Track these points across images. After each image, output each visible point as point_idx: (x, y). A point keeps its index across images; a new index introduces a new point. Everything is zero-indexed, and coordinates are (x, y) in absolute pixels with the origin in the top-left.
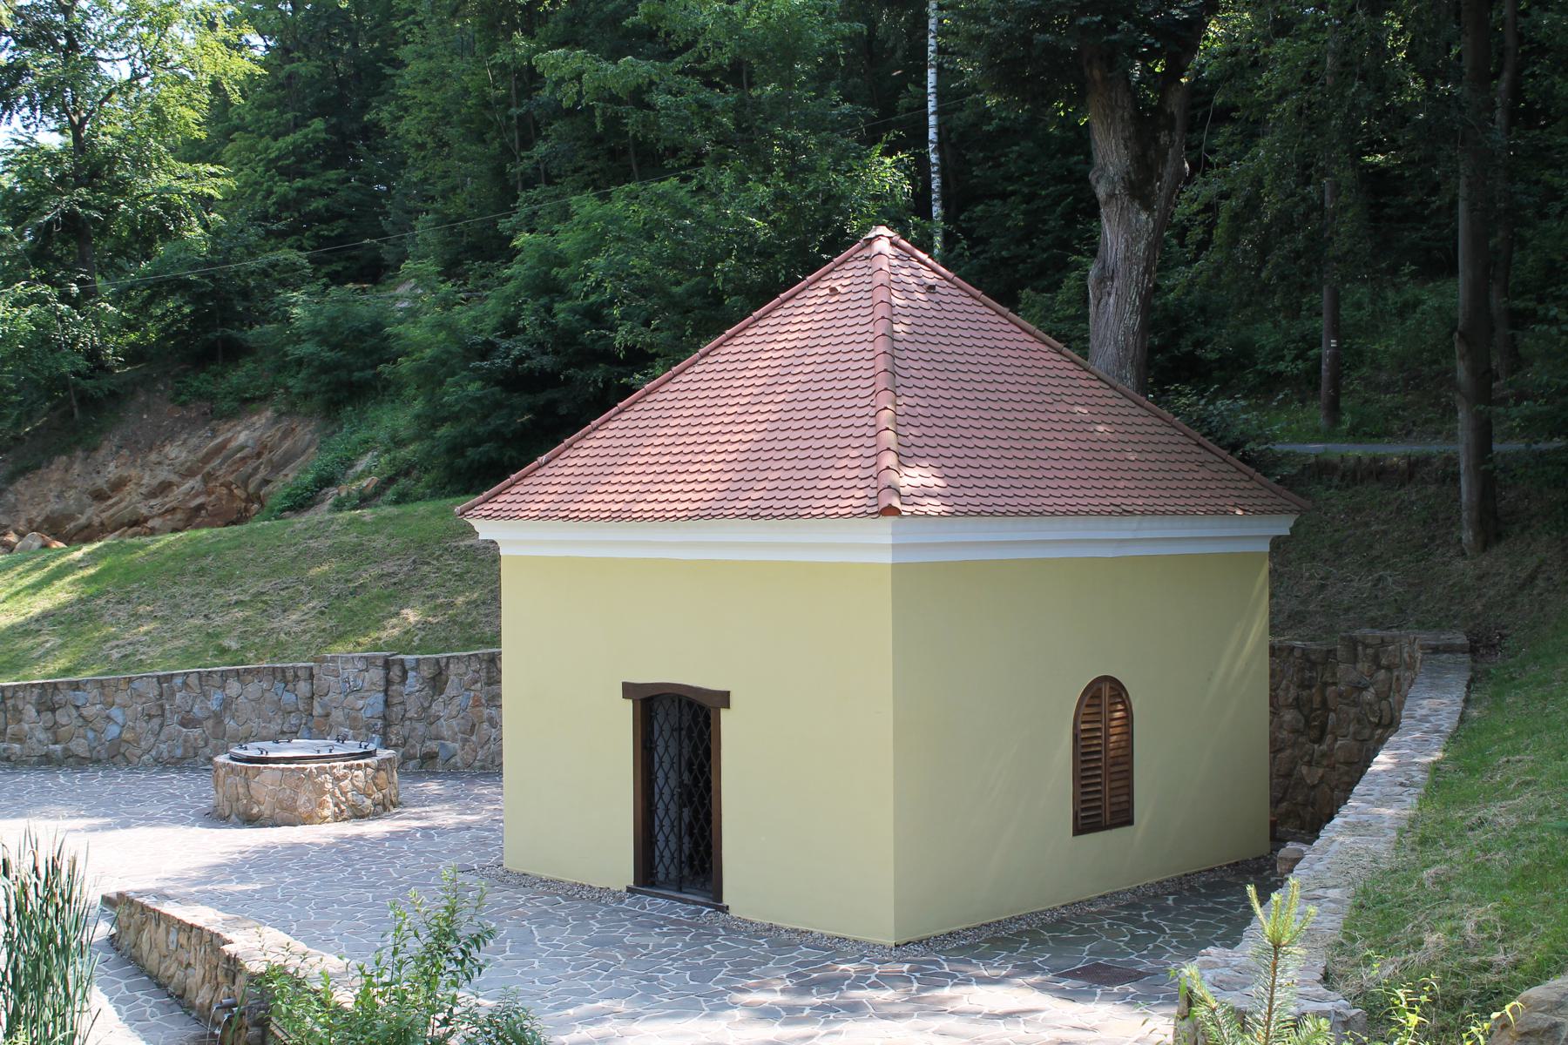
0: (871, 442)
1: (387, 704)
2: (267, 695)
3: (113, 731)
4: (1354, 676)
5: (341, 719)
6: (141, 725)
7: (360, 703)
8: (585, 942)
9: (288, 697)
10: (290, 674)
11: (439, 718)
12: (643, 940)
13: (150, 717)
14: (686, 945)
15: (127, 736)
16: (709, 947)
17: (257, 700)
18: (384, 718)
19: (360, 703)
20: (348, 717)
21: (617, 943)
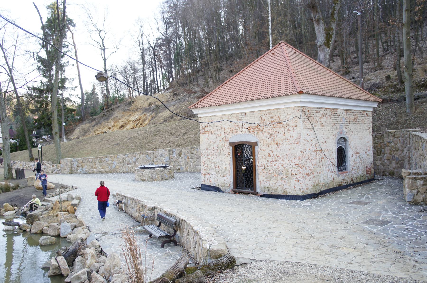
3: (114, 166)
4: (388, 140)
7: (164, 159)
9: (149, 158)
10: (149, 153)
15: (117, 167)
19: (164, 159)
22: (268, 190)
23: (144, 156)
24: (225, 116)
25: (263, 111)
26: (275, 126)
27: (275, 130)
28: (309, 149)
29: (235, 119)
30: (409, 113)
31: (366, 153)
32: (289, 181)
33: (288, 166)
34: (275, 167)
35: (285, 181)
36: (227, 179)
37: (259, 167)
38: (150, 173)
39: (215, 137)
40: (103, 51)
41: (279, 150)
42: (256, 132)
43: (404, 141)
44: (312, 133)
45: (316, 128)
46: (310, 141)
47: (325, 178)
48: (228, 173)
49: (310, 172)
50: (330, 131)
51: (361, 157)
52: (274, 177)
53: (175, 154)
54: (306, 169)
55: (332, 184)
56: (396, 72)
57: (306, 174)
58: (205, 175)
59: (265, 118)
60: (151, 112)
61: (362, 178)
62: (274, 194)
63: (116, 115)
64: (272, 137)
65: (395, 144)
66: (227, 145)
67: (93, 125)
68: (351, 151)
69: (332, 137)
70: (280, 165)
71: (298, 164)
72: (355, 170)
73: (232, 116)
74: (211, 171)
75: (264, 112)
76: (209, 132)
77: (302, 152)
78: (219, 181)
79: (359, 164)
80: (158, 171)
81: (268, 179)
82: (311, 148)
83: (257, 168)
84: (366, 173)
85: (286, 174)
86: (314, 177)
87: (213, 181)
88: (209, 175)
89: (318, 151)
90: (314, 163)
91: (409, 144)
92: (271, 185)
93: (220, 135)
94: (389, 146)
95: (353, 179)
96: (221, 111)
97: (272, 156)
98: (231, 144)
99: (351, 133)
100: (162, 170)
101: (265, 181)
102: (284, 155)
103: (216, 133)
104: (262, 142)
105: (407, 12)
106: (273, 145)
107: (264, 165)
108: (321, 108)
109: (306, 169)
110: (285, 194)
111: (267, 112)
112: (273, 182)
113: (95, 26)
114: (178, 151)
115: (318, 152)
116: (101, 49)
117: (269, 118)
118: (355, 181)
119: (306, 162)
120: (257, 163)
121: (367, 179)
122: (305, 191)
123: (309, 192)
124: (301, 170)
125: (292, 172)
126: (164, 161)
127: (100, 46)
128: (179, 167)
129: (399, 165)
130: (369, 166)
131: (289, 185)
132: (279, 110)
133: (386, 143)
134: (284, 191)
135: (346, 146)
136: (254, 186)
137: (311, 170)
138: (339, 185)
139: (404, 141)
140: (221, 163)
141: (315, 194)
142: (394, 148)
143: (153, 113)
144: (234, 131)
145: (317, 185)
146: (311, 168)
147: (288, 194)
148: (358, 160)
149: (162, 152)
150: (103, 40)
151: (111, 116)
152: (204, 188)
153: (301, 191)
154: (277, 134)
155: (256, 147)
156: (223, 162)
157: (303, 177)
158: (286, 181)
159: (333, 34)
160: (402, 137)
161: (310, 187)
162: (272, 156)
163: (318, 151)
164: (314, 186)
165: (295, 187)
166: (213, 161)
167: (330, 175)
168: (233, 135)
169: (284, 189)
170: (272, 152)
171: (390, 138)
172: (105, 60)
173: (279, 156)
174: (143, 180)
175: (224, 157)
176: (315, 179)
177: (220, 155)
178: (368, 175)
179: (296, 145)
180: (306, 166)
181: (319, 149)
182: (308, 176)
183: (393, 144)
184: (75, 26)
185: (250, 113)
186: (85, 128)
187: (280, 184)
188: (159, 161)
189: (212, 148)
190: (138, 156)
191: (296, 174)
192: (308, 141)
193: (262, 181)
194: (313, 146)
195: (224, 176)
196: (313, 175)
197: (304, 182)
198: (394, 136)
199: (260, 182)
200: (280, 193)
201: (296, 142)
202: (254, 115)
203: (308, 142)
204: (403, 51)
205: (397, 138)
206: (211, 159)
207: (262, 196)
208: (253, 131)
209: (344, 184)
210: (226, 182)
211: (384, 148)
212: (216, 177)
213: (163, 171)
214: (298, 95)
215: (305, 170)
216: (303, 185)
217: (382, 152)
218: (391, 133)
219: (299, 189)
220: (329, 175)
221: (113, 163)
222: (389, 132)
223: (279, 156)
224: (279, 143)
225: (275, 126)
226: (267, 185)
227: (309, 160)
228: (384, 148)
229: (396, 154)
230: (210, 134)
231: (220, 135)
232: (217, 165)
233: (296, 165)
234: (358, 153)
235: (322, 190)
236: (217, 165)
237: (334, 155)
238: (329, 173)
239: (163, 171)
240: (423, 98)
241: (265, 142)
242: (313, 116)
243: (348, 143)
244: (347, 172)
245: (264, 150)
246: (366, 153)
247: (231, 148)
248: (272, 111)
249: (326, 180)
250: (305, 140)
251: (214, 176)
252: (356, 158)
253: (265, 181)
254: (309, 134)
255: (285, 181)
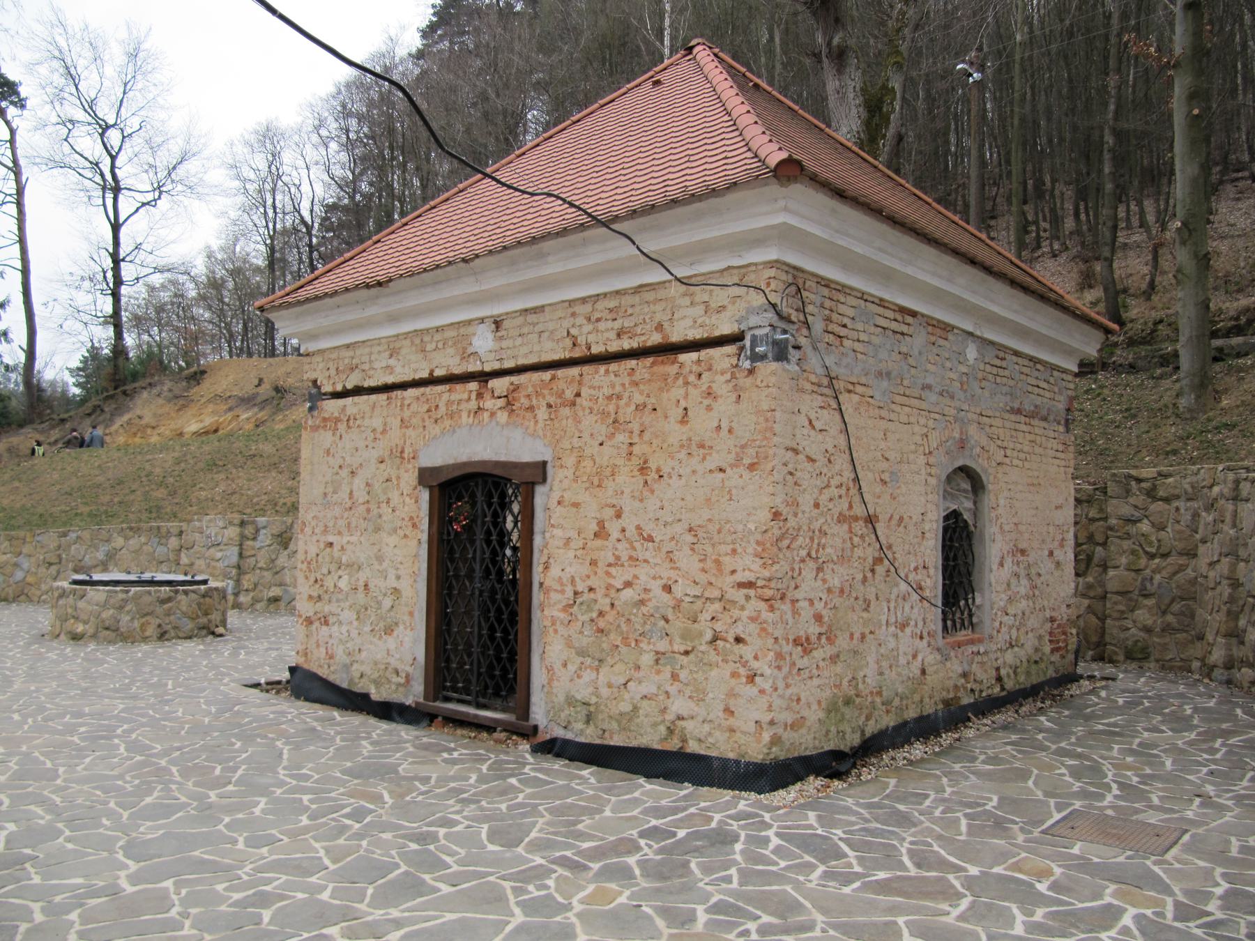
0: (740, 139)
1: (241, 555)
2: (145, 547)
3: (19, 575)
4: (1126, 510)
5: (203, 567)
6: (42, 570)
7: (219, 555)
8: (345, 772)
9: (161, 550)
10: (164, 530)
11: (283, 568)
12: (424, 771)
13: (50, 564)
14: (482, 779)
15: (30, 579)
16: (513, 781)
17: (136, 552)
18: (239, 567)
19: (219, 555)
20: (208, 565)
21: (387, 772)
22: (589, 719)
23: (143, 539)
24: (407, 343)
25: (584, 300)
26: (637, 377)
27: (638, 398)
28: (817, 505)
29: (451, 351)
30: (1190, 410)
31: (1051, 554)
32: (700, 676)
33: (697, 591)
34: (628, 594)
35: (675, 677)
36: (392, 646)
37: (547, 592)
38: (105, 606)
39: (361, 444)
40: (109, 196)
41: (652, 503)
42: (542, 413)
43: (1196, 515)
44: (828, 418)
45: (856, 398)
46: (822, 461)
47: (884, 664)
48: (406, 618)
49: (814, 629)
50: (917, 429)
51: (1033, 571)
52: (623, 649)
53: (265, 538)
54: (795, 612)
55: (917, 698)
56: (1096, 293)
57: (797, 642)
58: (309, 622)
59: (591, 338)
60: (256, 409)
61: (1034, 667)
62: (617, 740)
63: (138, 412)
64: (621, 438)
65: (1153, 525)
66: (410, 477)
67: (53, 439)
68: (999, 537)
69: (922, 460)
70: (656, 586)
71: (750, 585)
72: (1011, 627)
73: (437, 337)
74: (333, 607)
75: (587, 308)
76: (338, 420)
77: (776, 515)
78: (364, 654)
79: (1024, 603)
80: (147, 599)
81: (588, 661)
82: (823, 499)
83: (537, 596)
84: (1047, 649)
85: (685, 636)
86: (834, 659)
87: (340, 652)
88: (326, 623)
89: (856, 519)
90: (836, 582)
91: (1234, 526)
92: (605, 692)
93: (384, 432)
94: (1128, 536)
95: (1003, 672)
96: (393, 319)
97: (615, 534)
98: (425, 476)
99: (999, 455)
100: (163, 596)
101: (572, 668)
102: (679, 528)
103: (367, 422)
104: (570, 461)
105: (1190, 14)
106: (620, 479)
107: (573, 581)
108: (882, 303)
109: (795, 612)
110: (673, 745)
111: (601, 305)
112: (614, 673)
113: (90, 107)
114: (276, 530)
115: (859, 527)
116: (104, 188)
117: (612, 335)
118: (1010, 684)
119: (794, 577)
120: (537, 569)
121: (1051, 673)
122: (788, 736)
123: (807, 742)
124: (766, 615)
125: (719, 626)
126: (220, 565)
127: (102, 175)
128: (275, 591)
129: (1170, 618)
130: (1063, 614)
131: (699, 696)
132: (661, 294)
133: (1113, 521)
134: (670, 731)
135: (976, 513)
136: (519, 688)
137: (818, 618)
138: (946, 703)
139: (1196, 515)
140: (376, 566)
141: (838, 755)
142: (1151, 544)
143: (262, 409)
144: (443, 409)
145: (848, 702)
146: (819, 606)
147: (693, 747)
148: (1023, 587)
149: (213, 531)
150: (113, 158)
151: (121, 415)
152: (306, 685)
153: (766, 737)
154: (648, 418)
155: (540, 491)
156: (385, 565)
157: (779, 656)
158: (683, 675)
159: (893, 111)
160: (1189, 500)
161: (814, 715)
162: (615, 534)
163: (856, 519)
164: (832, 709)
165: (729, 711)
166: (344, 559)
167: (910, 651)
168: (437, 430)
169: (670, 717)
170: (618, 516)
171: (1132, 500)
172: (116, 227)
173: (650, 539)
174: (76, 637)
175: (393, 540)
176: (838, 668)
177: (378, 529)
178: (1056, 658)
179: (747, 475)
180: (799, 594)
181: (859, 510)
182: (807, 652)
183: (1145, 527)
184: (23, 107)
185: (520, 320)
186: (22, 447)
187: (648, 688)
188: (200, 564)
189: (343, 495)
190: (119, 541)
191: (738, 640)
192: (812, 460)
193: (561, 674)
194: (834, 492)
195: (389, 630)
196: (830, 650)
197: (781, 685)
198: (1151, 494)
199: (550, 670)
200: (650, 737)
201: (747, 461)
202: (540, 327)
203: (808, 466)
204: (1173, 163)
205: (1167, 500)
206: (336, 548)
207: (553, 748)
208: (531, 408)
209: (966, 700)
210: (394, 663)
211: (1104, 544)
212: (354, 633)
213: (169, 600)
214: (774, 189)
215: (789, 616)
216: (777, 702)
217: (1096, 560)
218: (1139, 480)
219: (751, 727)
220: (904, 654)
221: (16, 565)
222: (1130, 476)
223: (650, 539)
224: (653, 465)
225: (637, 377)
226: (583, 692)
227: (811, 565)
228: (1104, 544)
229: (1157, 570)
230: (342, 427)
231: (384, 432)
232: (362, 577)
233: (741, 585)
234: (1023, 552)
235: (871, 728)
236: (362, 577)
237: (931, 550)
238: (906, 642)
239: (169, 600)
240: (1239, 355)
241: (587, 463)
242: (843, 332)
243: (988, 500)
244: (980, 641)
245: (576, 505)
246: (1051, 554)
247: (425, 495)
248: (627, 300)
249: (891, 675)
250: (796, 452)
251: (344, 629)
252: (1017, 575)
253: (572, 668)
254: (818, 425)
255: (675, 677)
